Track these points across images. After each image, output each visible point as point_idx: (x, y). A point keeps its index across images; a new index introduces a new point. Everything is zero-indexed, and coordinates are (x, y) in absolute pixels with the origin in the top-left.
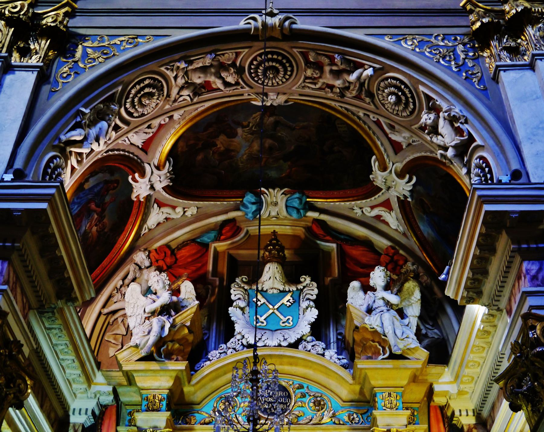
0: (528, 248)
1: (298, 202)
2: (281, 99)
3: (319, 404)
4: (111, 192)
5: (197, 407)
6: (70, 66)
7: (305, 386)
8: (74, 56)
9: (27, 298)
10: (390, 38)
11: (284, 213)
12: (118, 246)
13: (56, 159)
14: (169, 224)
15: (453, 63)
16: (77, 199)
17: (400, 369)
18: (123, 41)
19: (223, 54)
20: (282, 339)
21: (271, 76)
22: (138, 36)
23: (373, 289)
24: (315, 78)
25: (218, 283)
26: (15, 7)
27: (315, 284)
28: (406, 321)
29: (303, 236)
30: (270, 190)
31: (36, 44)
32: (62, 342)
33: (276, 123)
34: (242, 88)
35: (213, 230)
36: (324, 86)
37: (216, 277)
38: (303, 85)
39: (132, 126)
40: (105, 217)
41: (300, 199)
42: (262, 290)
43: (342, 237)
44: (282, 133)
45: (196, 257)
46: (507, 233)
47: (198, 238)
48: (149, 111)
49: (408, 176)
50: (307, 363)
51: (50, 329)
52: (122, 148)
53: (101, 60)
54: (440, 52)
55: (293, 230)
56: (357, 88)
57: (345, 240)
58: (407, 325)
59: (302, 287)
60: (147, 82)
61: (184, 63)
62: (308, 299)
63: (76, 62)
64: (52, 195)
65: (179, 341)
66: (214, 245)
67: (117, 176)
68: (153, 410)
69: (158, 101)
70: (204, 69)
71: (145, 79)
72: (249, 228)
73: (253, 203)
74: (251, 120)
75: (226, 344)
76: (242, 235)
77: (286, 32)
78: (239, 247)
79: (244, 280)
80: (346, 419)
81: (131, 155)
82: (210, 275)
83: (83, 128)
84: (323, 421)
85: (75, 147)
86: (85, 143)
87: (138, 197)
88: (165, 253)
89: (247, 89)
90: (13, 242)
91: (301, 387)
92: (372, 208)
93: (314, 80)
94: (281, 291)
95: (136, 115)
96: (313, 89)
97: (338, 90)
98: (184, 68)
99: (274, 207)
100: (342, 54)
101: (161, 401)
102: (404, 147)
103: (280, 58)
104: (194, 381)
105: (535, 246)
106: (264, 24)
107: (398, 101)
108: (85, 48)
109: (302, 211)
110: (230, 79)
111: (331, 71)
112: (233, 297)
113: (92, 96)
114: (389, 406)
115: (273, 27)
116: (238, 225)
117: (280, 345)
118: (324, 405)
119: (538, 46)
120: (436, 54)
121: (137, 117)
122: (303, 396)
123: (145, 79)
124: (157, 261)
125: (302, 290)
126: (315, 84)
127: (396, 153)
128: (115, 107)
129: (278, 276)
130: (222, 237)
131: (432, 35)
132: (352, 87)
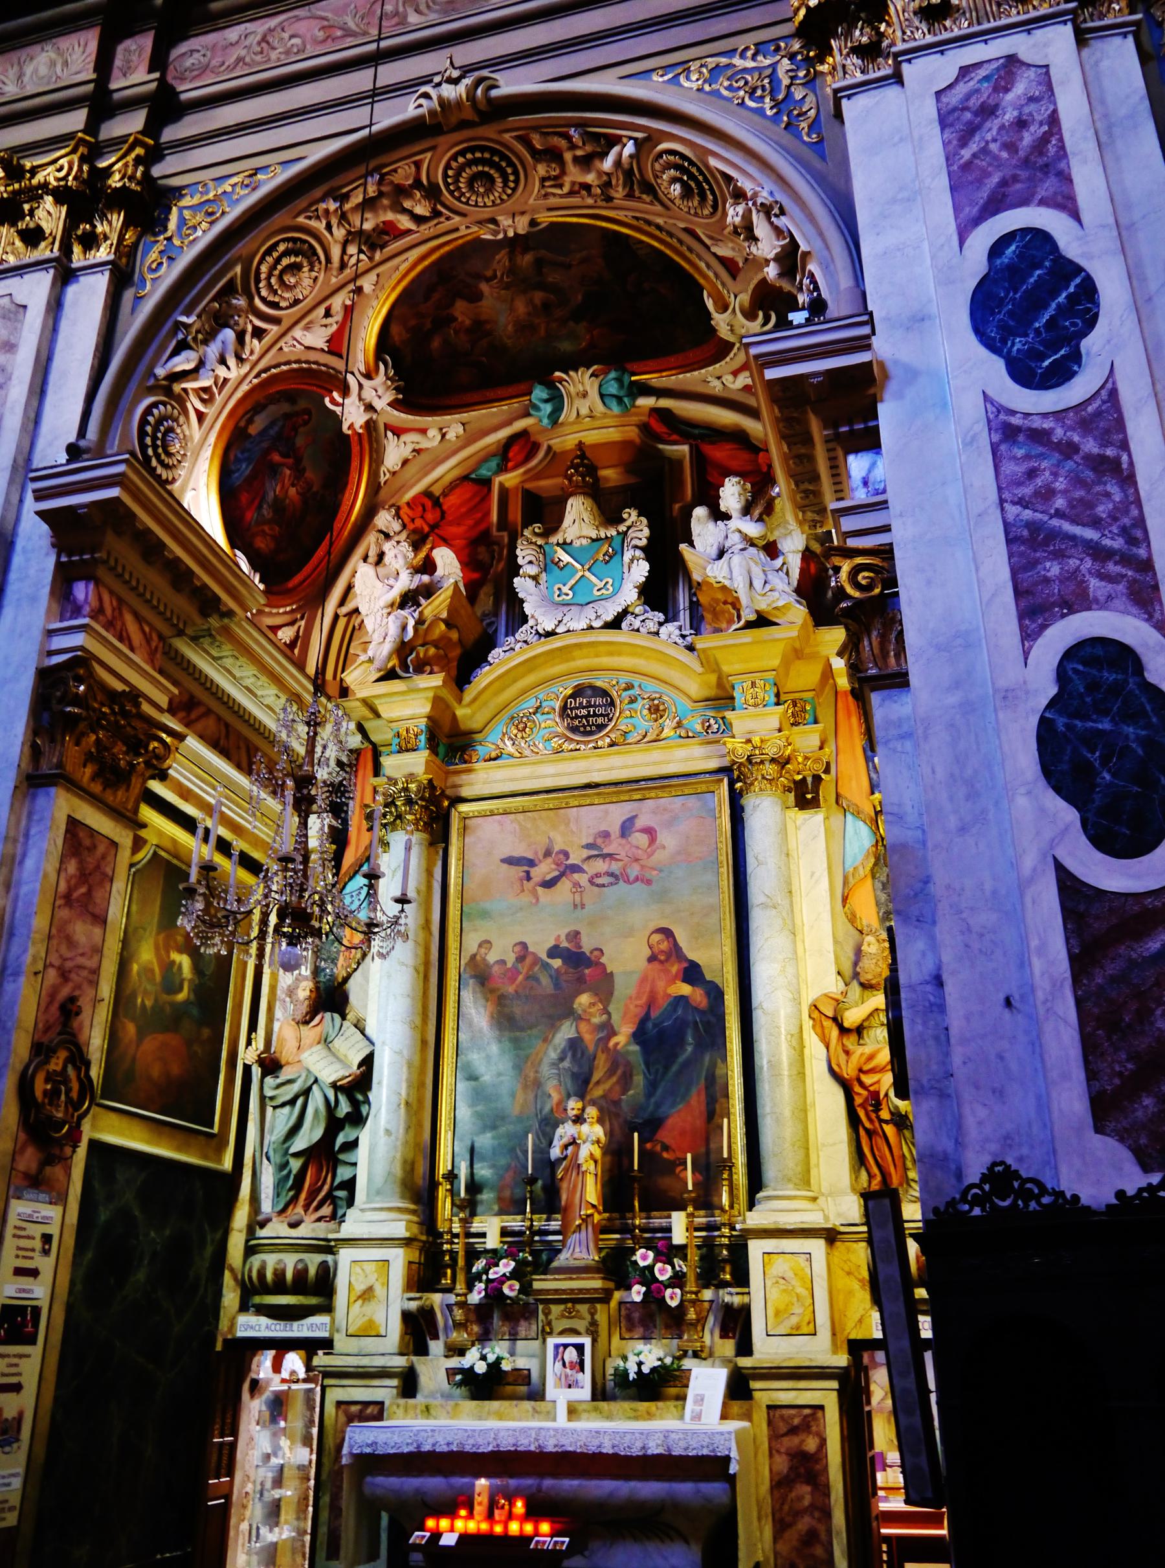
0: (852, 431)
1: (616, 385)
2: (522, 225)
3: (657, 710)
4: (301, 430)
5: (478, 737)
6: (162, 248)
7: (636, 684)
8: (166, 229)
9: (149, 624)
10: (662, 76)
11: (600, 407)
12: (345, 508)
13: (157, 408)
14: (424, 458)
15: (767, 100)
16: (242, 452)
17: (765, 641)
18: (236, 184)
19: (395, 171)
20: (593, 617)
21: (482, 190)
22: (257, 171)
23: (726, 517)
24: (556, 178)
25: (506, 540)
26: (60, 169)
27: (644, 520)
28: (778, 562)
29: (637, 440)
30: (572, 373)
31: (105, 223)
32: (247, 672)
33: (539, 263)
34: (448, 219)
35: (494, 455)
36: (576, 188)
37: (505, 530)
38: (543, 192)
39: (285, 324)
40: (304, 469)
41: (619, 380)
42: (565, 543)
43: (696, 431)
44: (553, 277)
45: (473, 503)
46: (816, 413)
47: (473, 471)
48: (305, 292)
49: (761, 314)
50: (635, 651)
51: (220, 658)
52: (293, 358)
53: (204, 225)
54: (746, 83)
55: (623, 432)
56: (621, 182)
57: (702, 437)
58: (781, 569)
59: (625, 529)
60: (282, 247)
61: (331, 201)
62: (636, 547)
63: (169, 239)
64: (122, 474)
65: (435, 644)
66: (498, 480)
67: (303, 404)
68: (407, 750)
69: (314, 274)
70: (369, 204)
71: (277, 244)
72: (552, 442)
73: (546, 401)
74: (495, 265)
75: (513, 635)
76: (541, 454)
77: (483, 106)
78: (538, 475)
79: (537, 530)
80: (699, 728)
81: (314, 366)
82: (494, 529)
83: (191, 348)
84: (663, 735)
85: (188, 381)
86: (202, 371)
87: (351, 427)
88: (423, 506)
89: (457, 219)
90: (92, 552)
91: (629, 687)
92: (735, 373)
93: (557, 182)
94: (593, 540)
95: (283, 304)
96: (561, 196)
97: (599, 191)
98: (336, 210)
99: (582, 400)
100: (581, 124)
101: (416, 736)
102: (741, 265)
103: (487, 155)
104: (465, 702)
105: (862, 426)
106: (441, 100)
107: (687, 193)
108: (181, 209)
109: (626, 400)
110: (420, 210)
111: (576, 160)
112: (520, 561)
113: (194, 292)
114: (751, 702)
115: (459, 103)
116: (532, 439)
117: (591, 628)
118: (664, 710)
119: (909, 33)
120: (739, 88)
121: (287, 308)
122: (633, 701)
123: (277, 244)
124: (413, 520)
125: (625, 533)
126: (561, 186)
127: (734, 277)
128: (241, 302)
129: (586, 516)
130: (510, 464)
131: (736, 50)
132: (614, 182)
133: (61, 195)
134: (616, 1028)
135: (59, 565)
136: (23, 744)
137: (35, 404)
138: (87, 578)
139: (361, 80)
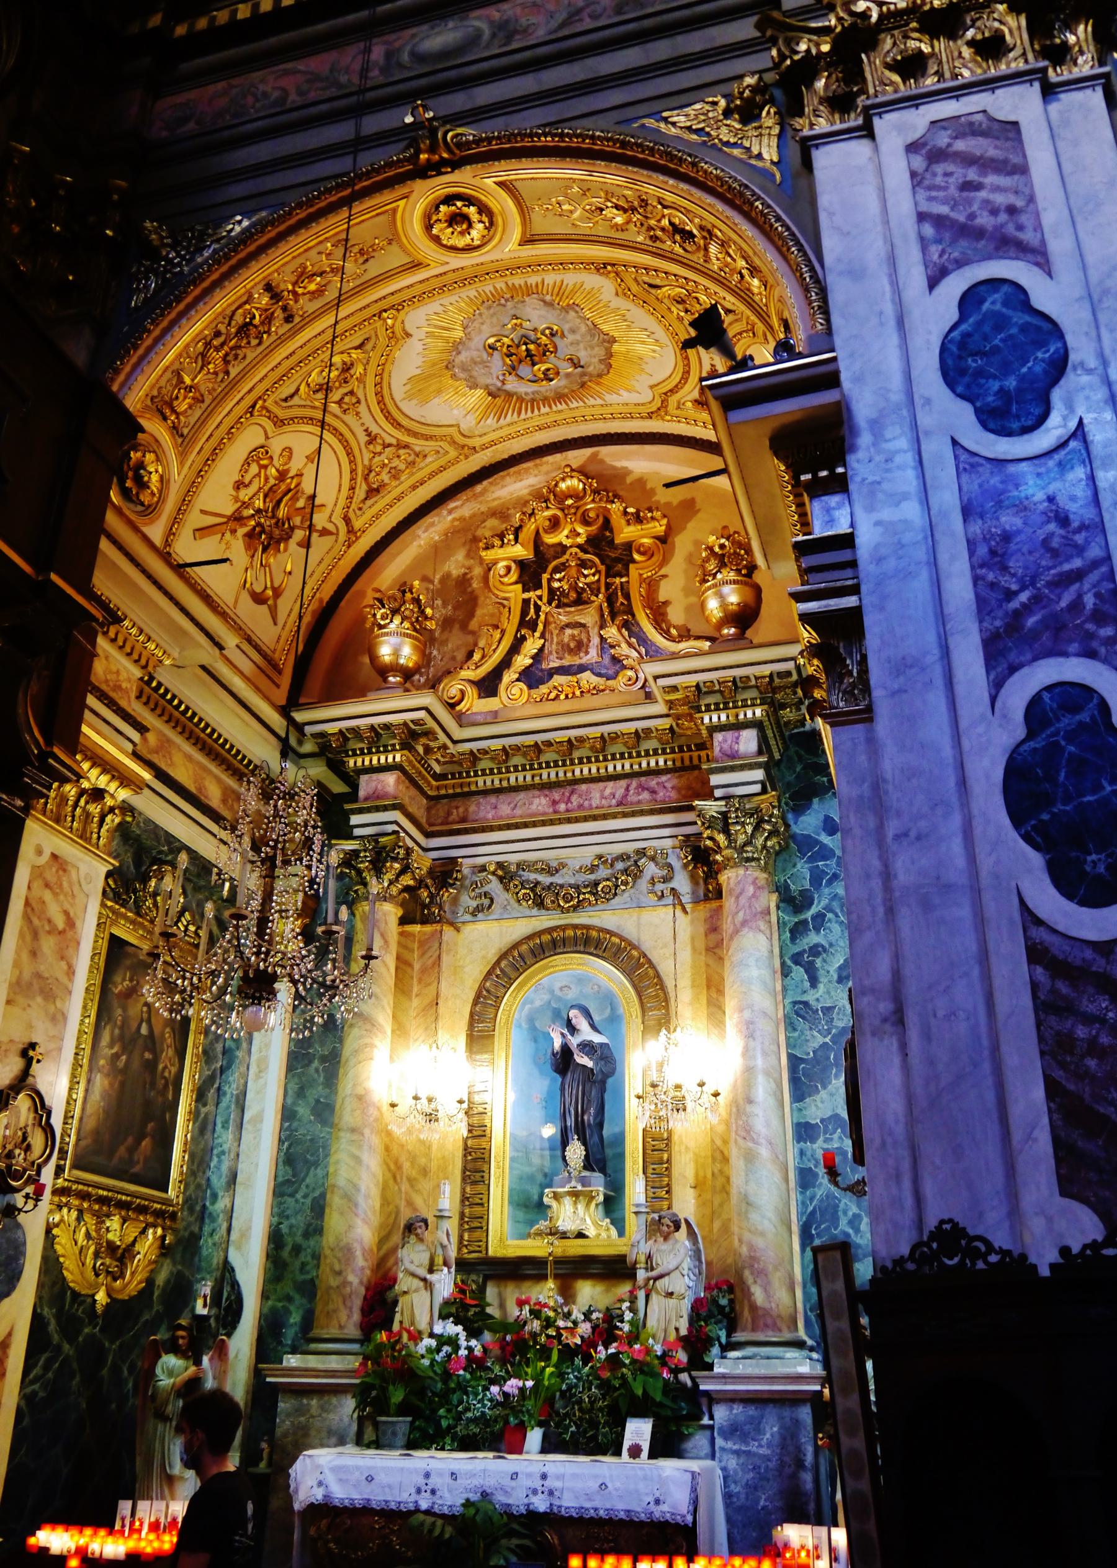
139: (341, 132)
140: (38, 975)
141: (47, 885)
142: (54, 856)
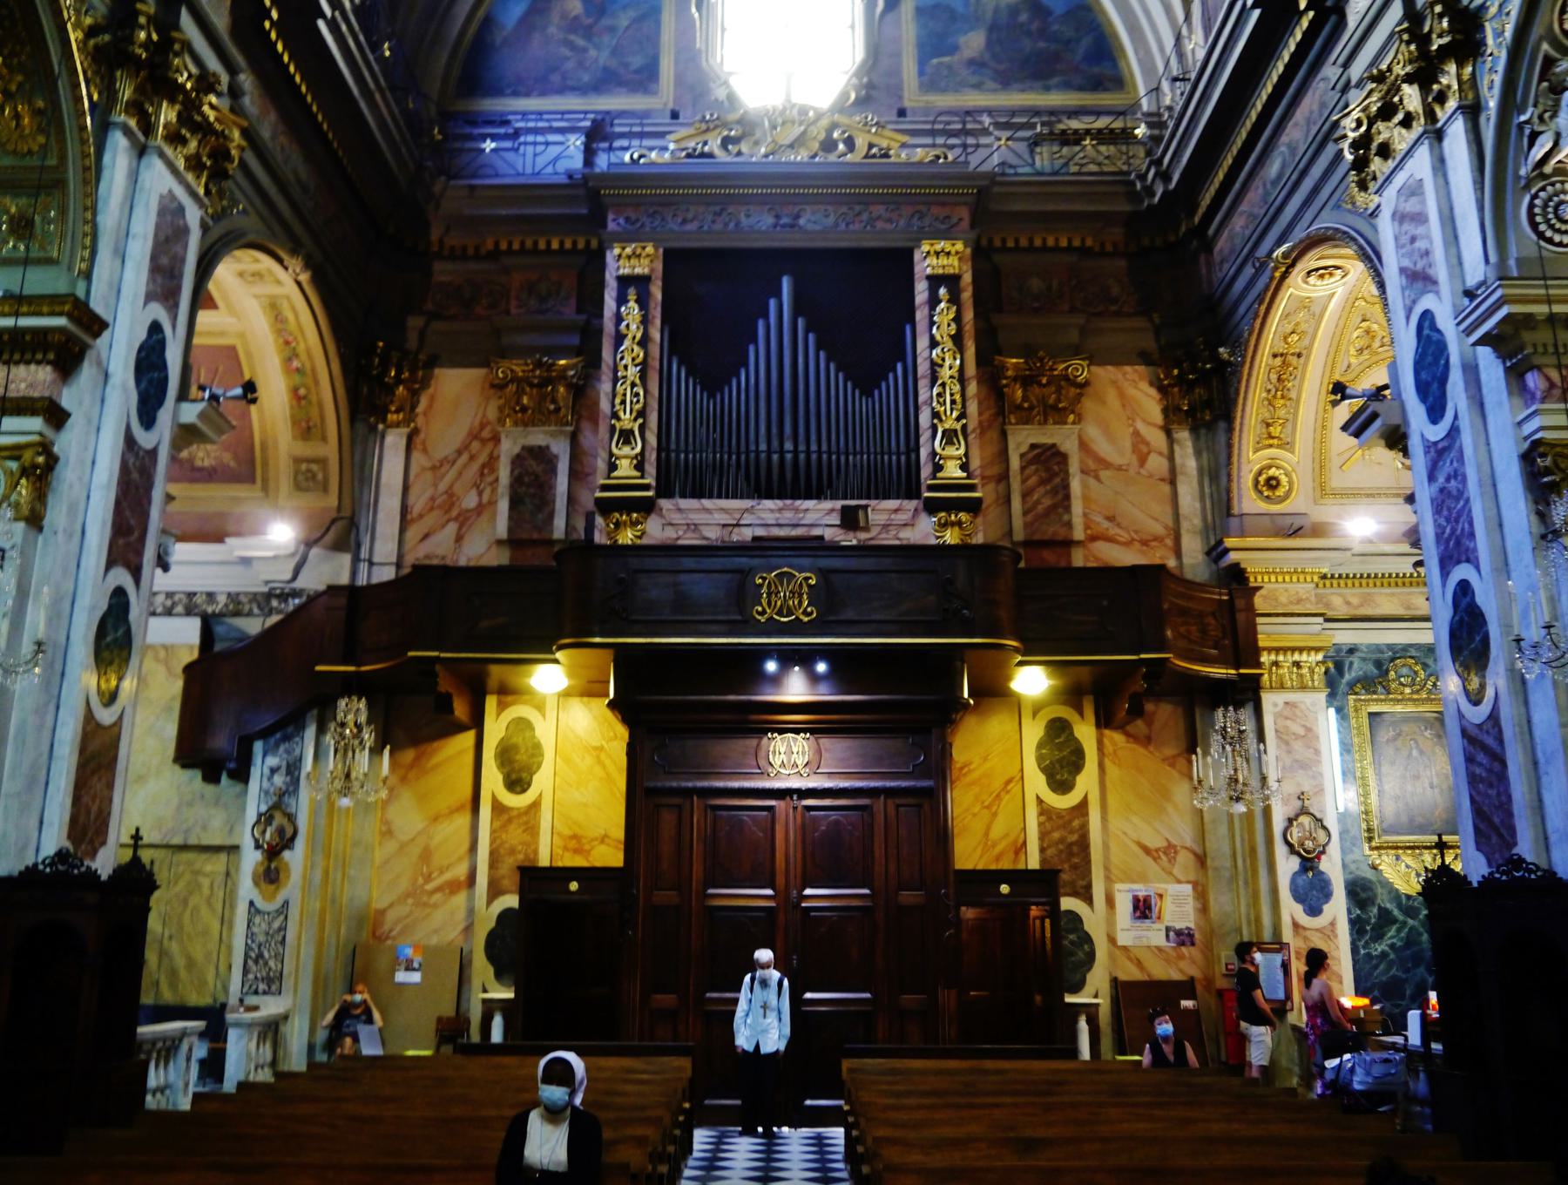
133: (1409, 79)
134: (517, 877)
135: (1508, 370)
136: (1528, 516)
137: (1453, 251)
138: (1532, 368)
140: (1297, 761)
141: (1287, 718)
142: (1286, 703)
